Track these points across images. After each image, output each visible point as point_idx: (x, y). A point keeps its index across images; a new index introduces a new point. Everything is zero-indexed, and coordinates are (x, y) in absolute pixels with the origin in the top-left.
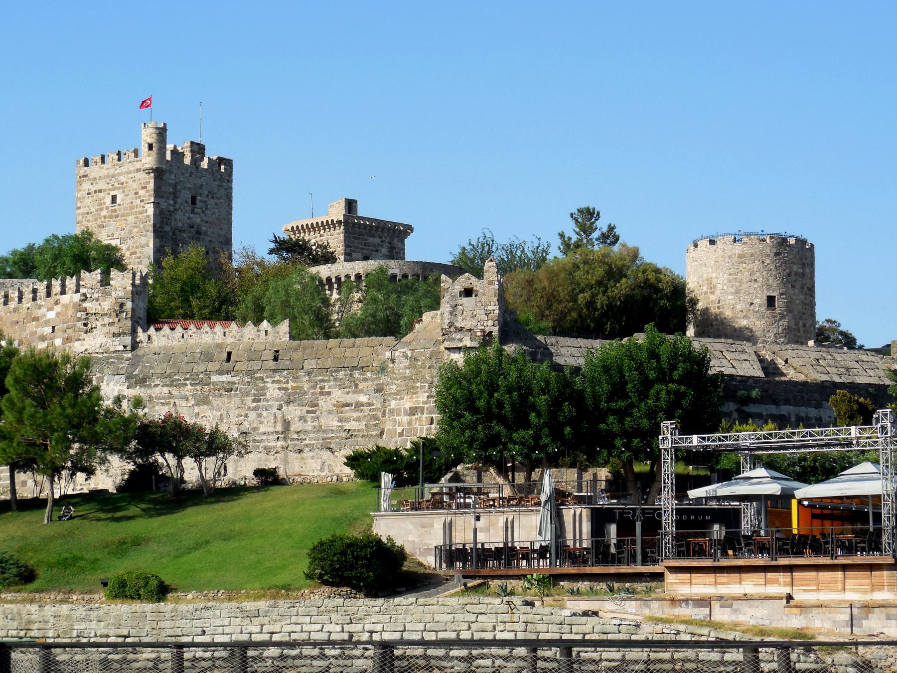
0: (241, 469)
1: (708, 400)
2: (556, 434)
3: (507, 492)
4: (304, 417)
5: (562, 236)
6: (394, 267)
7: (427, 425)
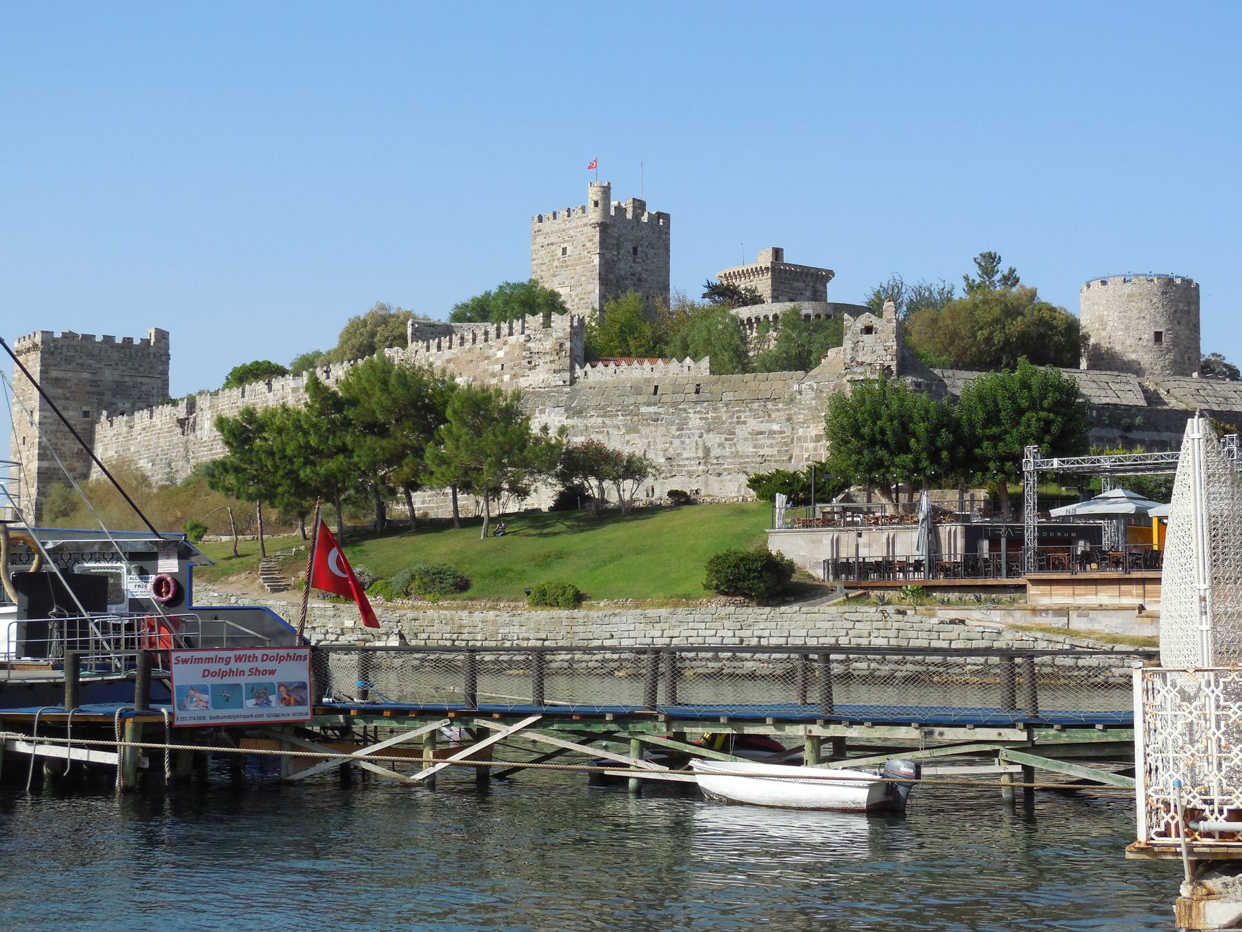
0: (662, 491)
1: (1070, 426)
2: (934, 457)
3: (890, 511)
4: (713, 443)
5: (966, 278)
6: (807, 308)
7: (823, 452)
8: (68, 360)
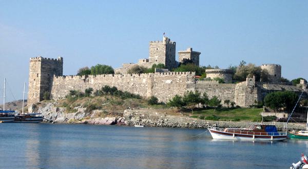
8: (46, 63)
